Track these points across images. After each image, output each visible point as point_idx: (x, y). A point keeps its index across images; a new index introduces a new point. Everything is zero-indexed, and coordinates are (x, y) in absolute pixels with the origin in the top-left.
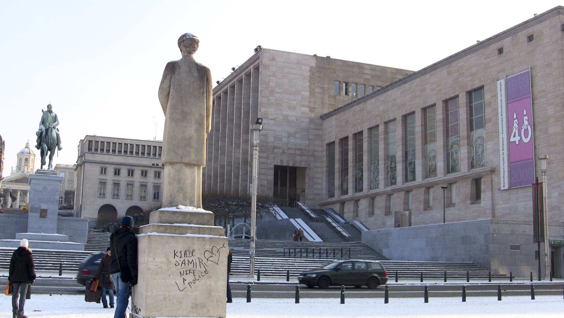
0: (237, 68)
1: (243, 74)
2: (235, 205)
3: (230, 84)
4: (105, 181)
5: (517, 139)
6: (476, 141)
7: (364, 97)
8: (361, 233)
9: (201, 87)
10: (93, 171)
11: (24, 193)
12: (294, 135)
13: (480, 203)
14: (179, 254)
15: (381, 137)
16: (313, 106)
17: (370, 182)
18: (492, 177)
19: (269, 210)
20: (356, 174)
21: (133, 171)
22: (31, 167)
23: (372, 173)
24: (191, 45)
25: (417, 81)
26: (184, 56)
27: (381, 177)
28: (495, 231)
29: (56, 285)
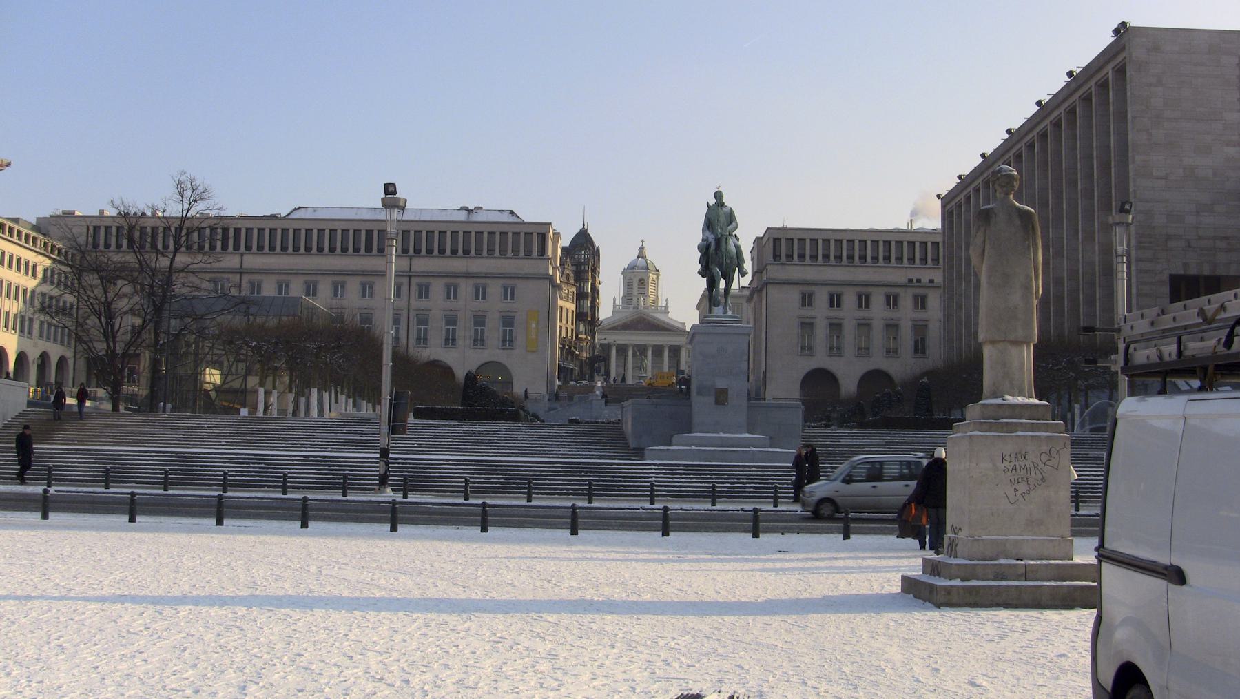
0: (1078, 72)
1: (1092, 83)
3: (1066, 105)
4: (812, 321)
10: (785, 301)
14: (1007, 458)
21: (868, 297)
22: (652, 297)
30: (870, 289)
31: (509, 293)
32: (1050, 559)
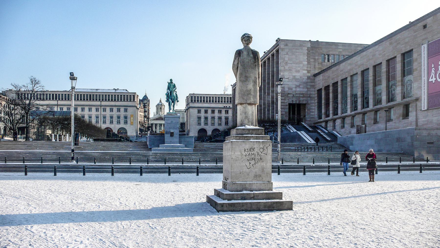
1: (270, 55)
2: (268, 126)
5: (434, 79)
6: (407, 82)
7: (338, 62)
8: (337, 137)
9: (255, 62)
10: (194, 112)
11: (161, 125)
12: (299, 86)
13: (408, 118)
14: (246, 150)
15: (349, 84)
16: (309, 70)
17: (342, 110)
18: (416, 103)
19: (286, 127)
20: (334, 105)
21: (214, 111)
23: (343, 104)
24: (248, 39)
25: (371, 50)
26: (244, 46)
27: (349, 106)
28: (418, 134)
29: (181, 169)
30: (214, 109)
31: (126, 110)
32: (263, 191)
